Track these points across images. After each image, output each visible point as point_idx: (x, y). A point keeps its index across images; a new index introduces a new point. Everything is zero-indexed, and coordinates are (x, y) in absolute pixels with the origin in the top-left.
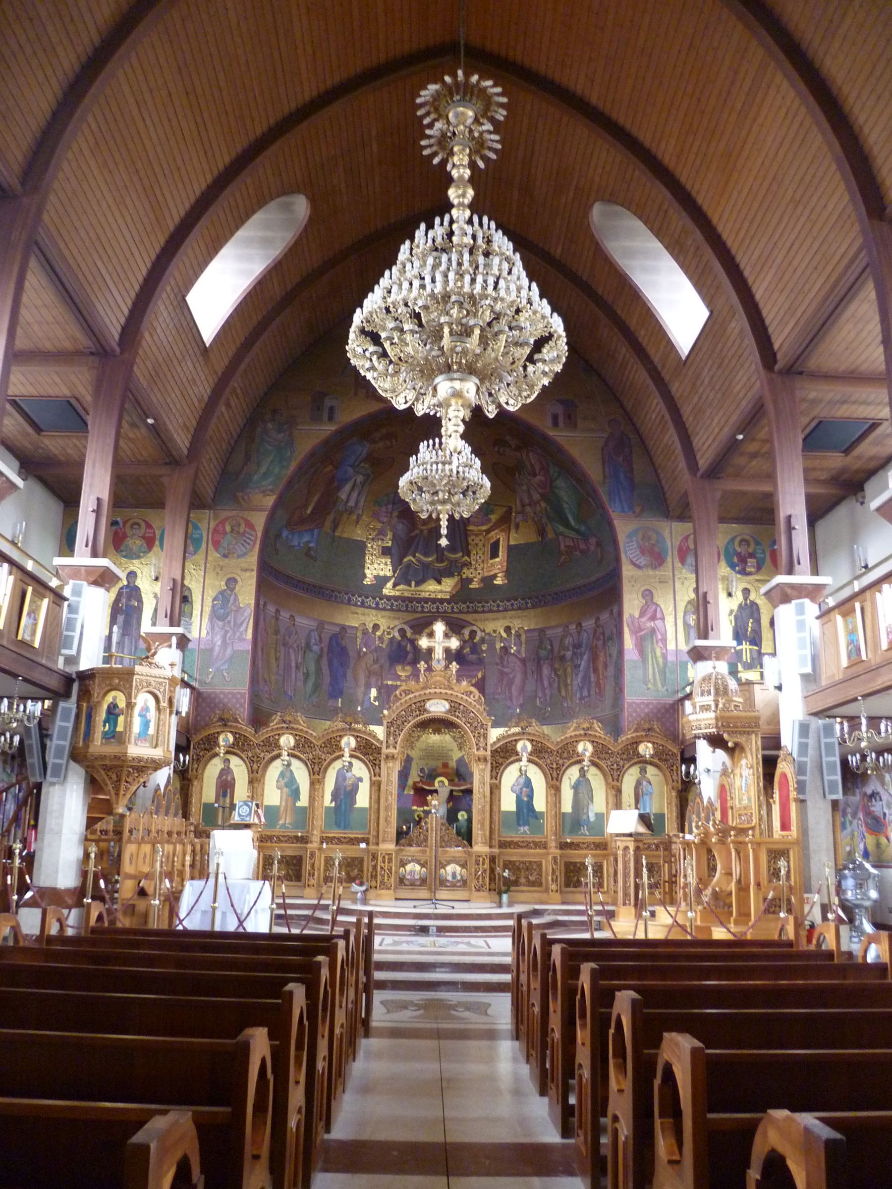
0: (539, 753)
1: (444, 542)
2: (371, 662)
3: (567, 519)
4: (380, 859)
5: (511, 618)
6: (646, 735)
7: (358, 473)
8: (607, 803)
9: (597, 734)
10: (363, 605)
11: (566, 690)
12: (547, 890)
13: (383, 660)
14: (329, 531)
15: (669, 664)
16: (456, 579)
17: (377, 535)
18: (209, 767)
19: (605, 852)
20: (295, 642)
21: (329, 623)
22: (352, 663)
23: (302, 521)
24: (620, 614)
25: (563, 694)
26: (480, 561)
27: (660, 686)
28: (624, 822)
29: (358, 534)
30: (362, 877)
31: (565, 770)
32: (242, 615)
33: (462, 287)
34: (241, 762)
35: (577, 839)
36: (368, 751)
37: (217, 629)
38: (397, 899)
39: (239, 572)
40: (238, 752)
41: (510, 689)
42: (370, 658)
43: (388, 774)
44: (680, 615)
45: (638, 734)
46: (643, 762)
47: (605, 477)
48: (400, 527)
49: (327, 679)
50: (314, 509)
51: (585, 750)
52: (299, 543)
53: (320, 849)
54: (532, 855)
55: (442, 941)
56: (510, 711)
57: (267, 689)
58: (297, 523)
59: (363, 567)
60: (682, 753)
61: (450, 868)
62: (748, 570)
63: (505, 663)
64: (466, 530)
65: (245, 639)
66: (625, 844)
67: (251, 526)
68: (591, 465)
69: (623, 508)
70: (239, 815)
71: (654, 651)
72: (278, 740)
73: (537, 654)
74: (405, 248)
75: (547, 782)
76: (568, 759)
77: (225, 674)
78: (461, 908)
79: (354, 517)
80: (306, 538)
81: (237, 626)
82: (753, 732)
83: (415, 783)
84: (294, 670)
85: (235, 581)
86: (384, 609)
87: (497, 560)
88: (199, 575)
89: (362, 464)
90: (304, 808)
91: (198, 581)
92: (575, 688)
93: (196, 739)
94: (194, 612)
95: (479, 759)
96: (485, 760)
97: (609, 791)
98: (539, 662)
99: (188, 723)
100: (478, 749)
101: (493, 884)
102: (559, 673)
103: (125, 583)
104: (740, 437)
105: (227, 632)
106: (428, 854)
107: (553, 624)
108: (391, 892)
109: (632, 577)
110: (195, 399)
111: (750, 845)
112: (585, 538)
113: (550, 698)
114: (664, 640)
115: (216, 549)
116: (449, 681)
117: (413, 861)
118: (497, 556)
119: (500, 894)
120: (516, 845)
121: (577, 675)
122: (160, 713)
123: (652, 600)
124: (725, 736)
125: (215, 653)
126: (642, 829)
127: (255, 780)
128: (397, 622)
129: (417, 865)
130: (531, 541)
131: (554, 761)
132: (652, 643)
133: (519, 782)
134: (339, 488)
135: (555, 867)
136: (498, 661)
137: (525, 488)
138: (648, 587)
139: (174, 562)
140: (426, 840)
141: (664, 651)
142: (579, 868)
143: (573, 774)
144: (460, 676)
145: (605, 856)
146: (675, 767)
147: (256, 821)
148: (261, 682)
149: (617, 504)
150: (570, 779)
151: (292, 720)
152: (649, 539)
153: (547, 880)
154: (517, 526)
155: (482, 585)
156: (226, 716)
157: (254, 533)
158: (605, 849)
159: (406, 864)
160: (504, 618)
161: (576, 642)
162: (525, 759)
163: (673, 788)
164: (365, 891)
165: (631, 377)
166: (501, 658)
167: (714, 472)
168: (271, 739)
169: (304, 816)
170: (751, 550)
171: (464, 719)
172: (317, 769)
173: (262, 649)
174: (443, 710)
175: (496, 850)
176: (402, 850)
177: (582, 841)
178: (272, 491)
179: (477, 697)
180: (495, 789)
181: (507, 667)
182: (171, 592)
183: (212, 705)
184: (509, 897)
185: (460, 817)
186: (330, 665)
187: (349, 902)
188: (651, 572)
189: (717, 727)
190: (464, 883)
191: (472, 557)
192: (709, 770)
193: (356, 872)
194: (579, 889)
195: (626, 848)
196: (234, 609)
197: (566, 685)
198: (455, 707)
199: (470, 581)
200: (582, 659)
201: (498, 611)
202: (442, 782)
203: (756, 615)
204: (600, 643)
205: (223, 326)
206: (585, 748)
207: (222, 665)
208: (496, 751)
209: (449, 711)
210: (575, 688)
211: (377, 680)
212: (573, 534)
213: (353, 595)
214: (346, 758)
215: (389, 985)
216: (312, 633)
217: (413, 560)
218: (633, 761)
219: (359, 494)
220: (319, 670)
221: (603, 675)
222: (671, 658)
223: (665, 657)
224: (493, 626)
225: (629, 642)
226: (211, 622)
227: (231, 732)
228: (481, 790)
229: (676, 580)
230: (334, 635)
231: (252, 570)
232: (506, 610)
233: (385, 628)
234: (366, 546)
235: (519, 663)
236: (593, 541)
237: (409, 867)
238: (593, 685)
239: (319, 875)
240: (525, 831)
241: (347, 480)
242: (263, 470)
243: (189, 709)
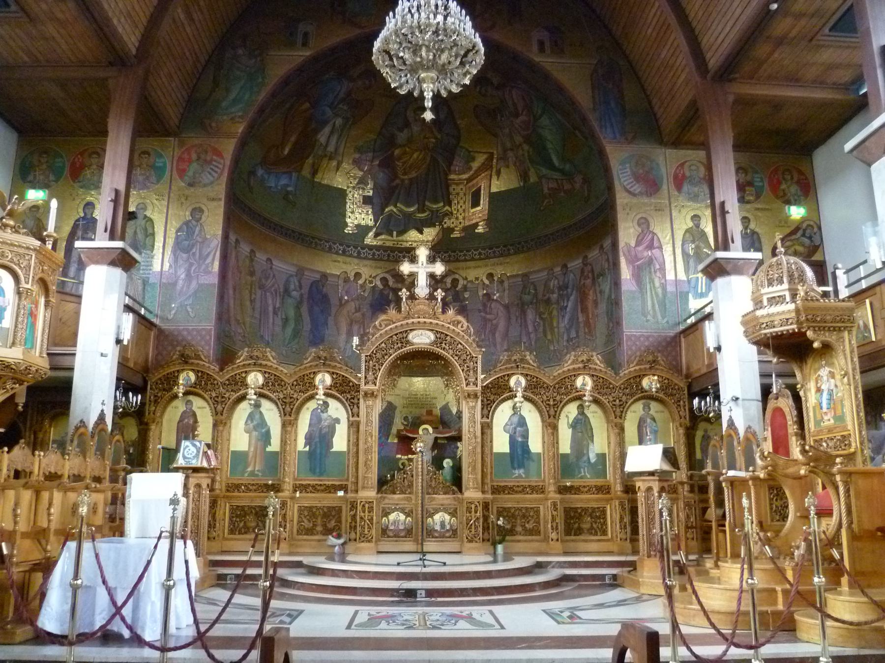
1: (428, 116)
2: (353, 311)
3: (551, 160)
4: (359, 508)
5: (494, 265)
7: (337, 115)
9: (597, 367)
11: (552, 333)
12: (546, 539)
13: (365, 309)
15: (669, 295)
17: (358, 183)
18: (169, 409)
19: (608, 496)
20: (273, 285)
22: (334, 310)
24: (615, 245)
25: (549, 337)
27: (660, 318)
28: (645, 457)
29: (339, 181)
30: (340, 529)
31: (563, 407)
33: (432, 78)
35: (577, 482)
36: (345, 390)
37: (181, 262)
38: (380, 552)
39: (205, 201)
41: (494, 334)
42: (352, 306)
43: (368, 413)
44: (678, 244)
45: (642, 367)
46: (649, 397)
48: (381, 175)
52: (276, 186)
53: (293, 498)
54: (528, 500)
55: (435, 613)
56: (494, 357)
59: (344, 216)
60: (689, 387)
61: (438, 517)
62: (747, 198)
64: (447, 180)
65: (210, 272)
66: (647, 485)
68: (582, 93)
70: (184, 457)
71: (652, 281)
72: (245, 378)
75: (543, 421)
76: (567, 394)
77: (189, 310)
78: (454, 563)
79: (334, 163)
80: (284, 181)
81: (203, 258)
82: (845, 328)
83: (399, 431)
84: (271, 314)
85: (201, 211)
86: (366, 258)
87: (479, 208)
88: (161, 205)
89: (341, 106)
90: (276, 453)
92: (562, 330)
93: (153, 378)
95: (469, 395)
96: (476, 396)
99: (147, 361)
100: (467, 385)
101: (486, 534)
102: (544, 316)
103: (82, 215)
104: (775, 6)
105: (191, 265)
107: (536, 268)
108: (372, 545)
109: (627, 204)
113: (536, 342)
114: (663, 269)
115: (181, 177)
116: (433, 309)
117: (396, 510)
118: (478, 204)
119: (494, 544)
120: (511, 490)
121: (563, 316)
122: (20, 298)
123: (648, 227)
124: (810, 334)
126: (667, 467)
127: (221, 423)
128: (379, 271)
129: (401, 514)
131: (549, 398)
132: (650, 272)
133: (512, 423)
134: (316, 131)
135: (555, 513)
137: (507, 131)
138: (644, 215)
139: (117, 173)
140: (411, 486)
141: (663, 281)
142: (580, 514)
143: (571, 411)
144: (445, 305)
146: (682, 403)
148: (233, 322)
149: (609, 130)
150: (567, 416)
151: (260, 355)
153: (545, 527)
154: (498, 173)
155: (463, 235)
157: (222, 161)
158: (608, 493)
159: (389, 513)
160: (486, 266)
162: (519, 394)
163: (681, 426)
166: (485, 305)
167: (729, 70)
168: (238, 377)
169: (274, 462)
170: (749, 178)
172: (288, 409)
174: (428, 341)
175: (489, 496)
176: (385, 498)
180: (487, 428)
181: (490, 314)
182: (112, 204)
184: (505, 548)
185: (445, 464)
186: (311, 312)
188: (646, 200)
189: (799, 322)
190: (454, 533)
192: (737, 399)
193: (333, 523)
194: (581, 537)
195: (649, 489)
196: (200, 240)
197: (552, 329)
198: (441, 338)
199: (452, 230)
200: (568, 300)
201: (480, 259)
202: (427, 429)
204: (588, 282)
207: (186, 300)
208: (487, 387)
209: (434, 343)
210: (562, 330)
211: (360, 327)
212: (557, 175)
213: (335, 244)
214: (321, 395)
216: (291, 279)
217: (395, 210)
219: (338, 139)
220: (299, 318)
222: (670, 288)
223: (664, 287)
225: (626, 273)
226: (175, 255)
227: (193, 370)
229: (673, 208)
230: (314, 282)
231: (220, 199)
232: (487, 258)
233: (367, 277)
234: (347, 195)
235: (502, 309)
236: (579, 179)
237: (392, 517)
238: (582, 325)
241: (325, 123)
242: (232, 96)
243: (132, 336)
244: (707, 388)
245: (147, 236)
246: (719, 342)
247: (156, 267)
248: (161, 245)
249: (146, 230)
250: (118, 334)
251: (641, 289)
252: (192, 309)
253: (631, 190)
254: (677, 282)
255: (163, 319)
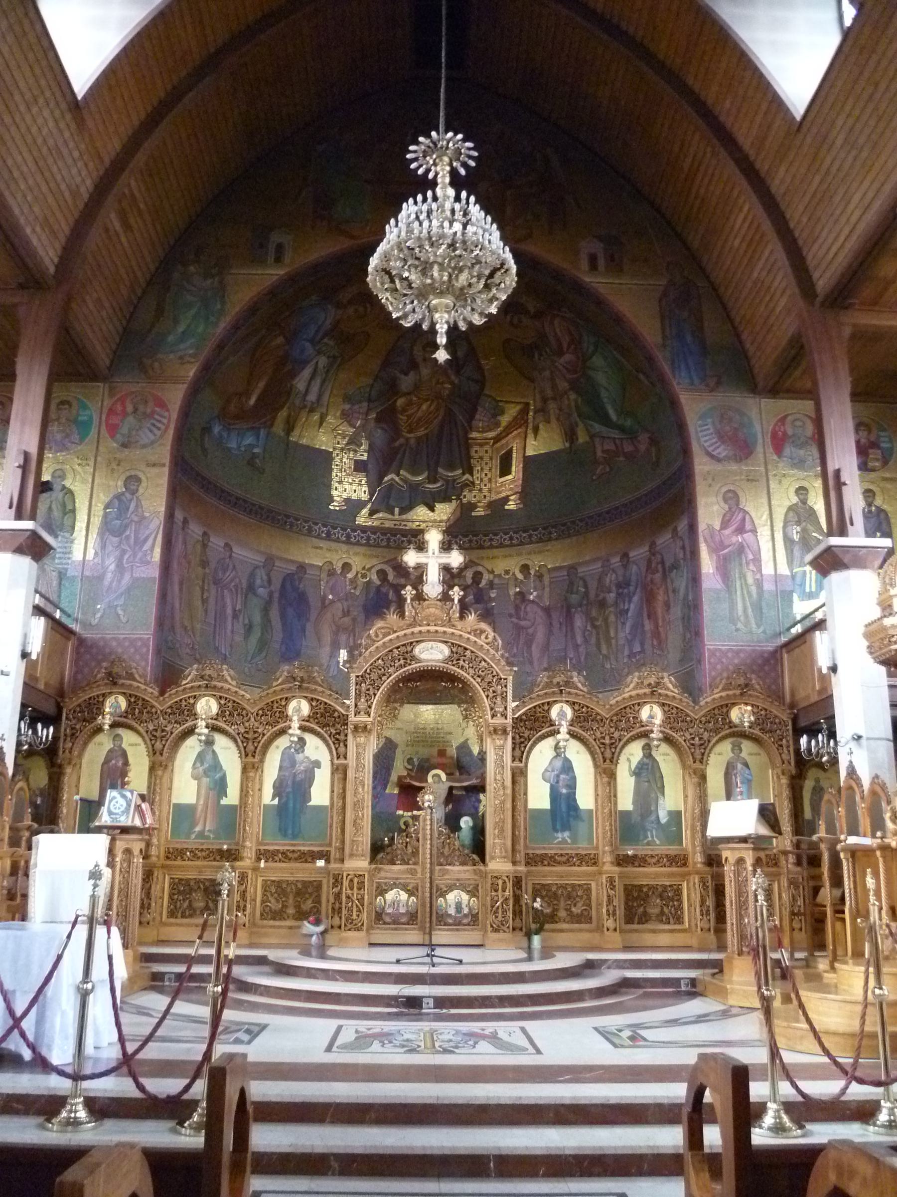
0: (584, 723)
1: (442, 356)
2: (340, 614)
4: (346, 883)
5: (530, 553)
6: (742, 694)
7: (319, 352)
8: (686, 796)
9: (669, 693)
10: (328, 537)
11: (609, 645)
12: (600, 929)
14: (282, 434)
15: (766, 595)
16: (454, 504)
17: (347, 444)
18: (91, 746)
19: (684, 869)
20: (232, 581)
21: (281, 559)
22: (313, 616)
23: (242, 415)
24: (693, 527)
25: (604, 651)
26: (486, 480)
27: (754, 626)
28: (734, 818)
29: (323, 440)
30: (319, 912)
31: (623, 747)
32: (147, 527)
33: (447, 306)
34: (139, 740)
36: (328, 722)
37: (110, 548)
38: (372, 945)
39: (143, 467)
40: (134, 723)
43: (358, 754)
45: (730, 693)
47: (664, 337)
49: (278, 634)
50: (258, 399)
51: (651, 717)
52: (239, 447)
53: (256, 869)
54: (576, 874)
55: (447, 1030)
57: (187, 641)
58: (236, 416)
59: (329, 487)
60: (795, 720)
61: (452, 897)
62: (870, 464)
63: (522, 614)
64: (468, 439)
66: (738, 855)
67: (162, 404)
69: (692, 384)
70: (110, 813)
71: (743, 577)
73: (566, 599)
74: (387, 227)
75: (596, 766)
77: (120, 612)
79: (316, 417)
80: (249, 440)
81: (139, 543)
83: (400, 778)
84: (230, 619)
86: (358, 544)
87: (510, 477)
88: (85, 472)
89: (326, 340)
90: (233, 808)
91: (84, 481)
93: (71, 704)
94: (78, 524)
95: (495, 731)
96: (505, 732)
97: (687, 778)
98: (568, 611)
100: (493, 716)
102: (598, 623)
105: (124, 552)
106: (419, 875)
108: (362, 934)
109: (708, 472)
110: (67, 194)
111: (878, 853)
112: (631, 435)
113: (586, 658)
114: (757, 560)
115: (112, 436)
119: (529, 935)
120: (552, 860)
121: (624, 624)
125: (106, 583)
126: (764, 831)
127: (160, 765)
128: (375, 561)
129: (402, 893)
130: (554, 449)
131: (604, 736)
132: (741, 565)
133: (555, 768)
134: (293, 375)
136: (513, 612)
137: (547, 373)
140: (415, 853)
141: (758, 576)
143: (634, 753)
145: (684, 876)
147: (138, 823)
148: (179, 630)
151: (215, 675)
152: (730, 420)
154: (536, 430)
156: (115, 670)
157: (166, 414)
158: (685, 865)
159: (386, 891)
160: (520, 554)
161: (621, 579)
162: (564, 730)
163: (783, 774)
164: (323, 933)
165: (702, 191)
166: (517, 608)
167: (842, 296)
168: (184, 703)
169: (231, 820)
171: (471, 671)
172: (251, 747)
173: (181, 583)
174: (440, 657)
175: (522, 868)
176: (380, 869)
177: (650, 853)
178: (194, 356)
179: (491, 637)
180: (519, 775)
182: (19, 471)
183: (94, 651)
184: (543, 941)
185: (462, 824)
186: (283, 616)
187: (294, 953)
188: (734, 467)
190: (474, 919)
191: (476, 475)
192: (860, 737)
195: (740, 861)
196: (136, 519)
197: (608, 640)
198: (458, 653)
199: (472, 506)
200: (630, 602)
201: (512, 545)
202: (438, 776)
203: (884, 526)
204: (658, 576)
205: (104, 71)
206: (652, 714)
208: (519, 719)
209: (449, 660)
210: (621, 642)
211: (348, 639)
212: (615, 434)
214: (295, 730)
215: (335, 1165)
217: (397, 479)
218: (723, 733)
221: (664, 620)
222: (768, 586)
223: (759, 584)
224: (505, 565)
225: (707, 564)
226: (102, 539)
228: (498, 777)
230: (288, 575)
231: (164, 465)
232: (521, 544)
236: (644, 437)
237: (390, 896)
238: (649, 635)
239: (254, 909)
240: (563, 839)
241: (304, 363)
242: (181, 329)
244: (819, 723)
245: (65, 514)
246: (834, 659)
247: (77, 554)
248: (84, 525)
249: (64, 505)
250: (24, 644)
251: (727, 586)
252: (124, 611)
253: (714, 453)
254: (777, 578)
255: (86, 625)
